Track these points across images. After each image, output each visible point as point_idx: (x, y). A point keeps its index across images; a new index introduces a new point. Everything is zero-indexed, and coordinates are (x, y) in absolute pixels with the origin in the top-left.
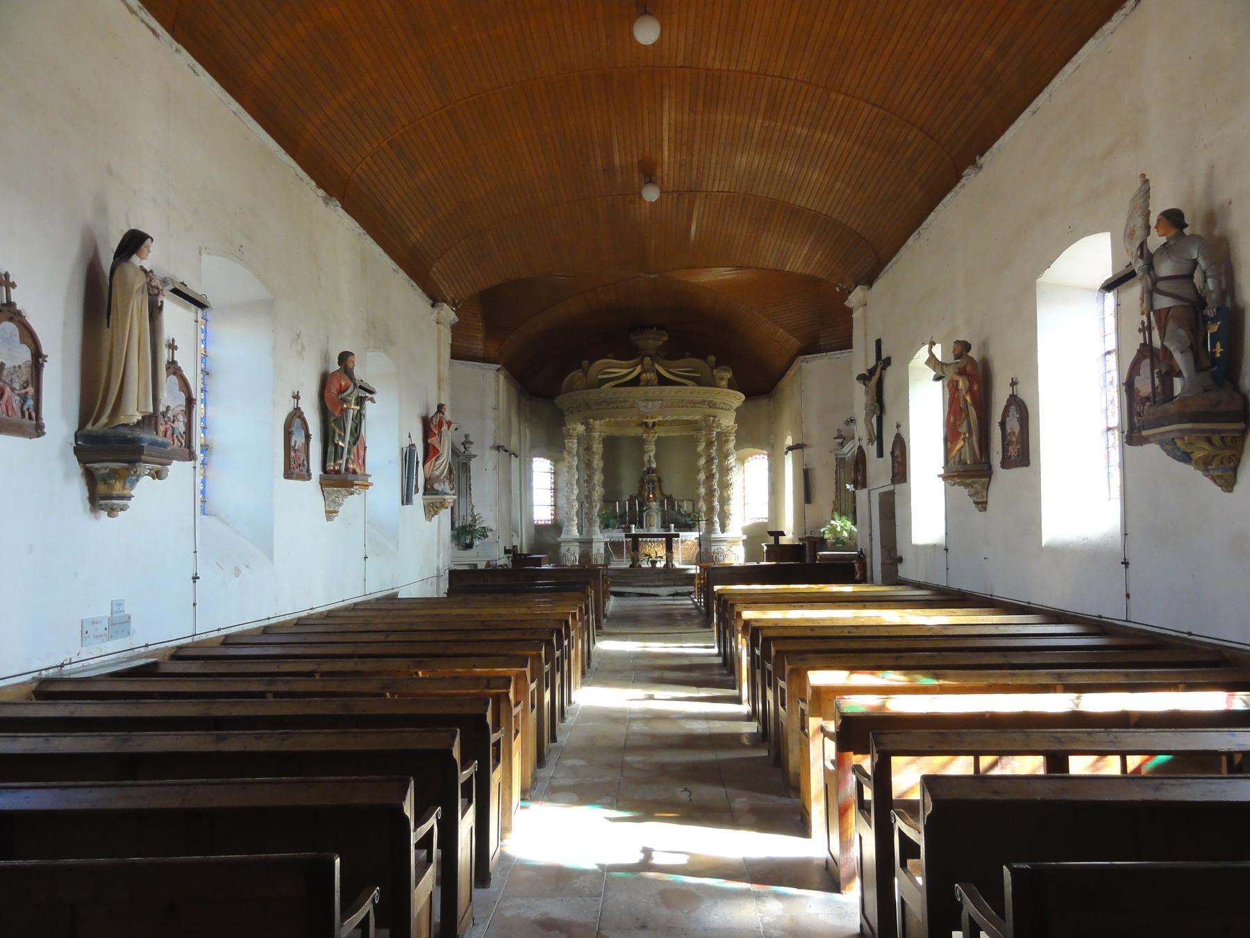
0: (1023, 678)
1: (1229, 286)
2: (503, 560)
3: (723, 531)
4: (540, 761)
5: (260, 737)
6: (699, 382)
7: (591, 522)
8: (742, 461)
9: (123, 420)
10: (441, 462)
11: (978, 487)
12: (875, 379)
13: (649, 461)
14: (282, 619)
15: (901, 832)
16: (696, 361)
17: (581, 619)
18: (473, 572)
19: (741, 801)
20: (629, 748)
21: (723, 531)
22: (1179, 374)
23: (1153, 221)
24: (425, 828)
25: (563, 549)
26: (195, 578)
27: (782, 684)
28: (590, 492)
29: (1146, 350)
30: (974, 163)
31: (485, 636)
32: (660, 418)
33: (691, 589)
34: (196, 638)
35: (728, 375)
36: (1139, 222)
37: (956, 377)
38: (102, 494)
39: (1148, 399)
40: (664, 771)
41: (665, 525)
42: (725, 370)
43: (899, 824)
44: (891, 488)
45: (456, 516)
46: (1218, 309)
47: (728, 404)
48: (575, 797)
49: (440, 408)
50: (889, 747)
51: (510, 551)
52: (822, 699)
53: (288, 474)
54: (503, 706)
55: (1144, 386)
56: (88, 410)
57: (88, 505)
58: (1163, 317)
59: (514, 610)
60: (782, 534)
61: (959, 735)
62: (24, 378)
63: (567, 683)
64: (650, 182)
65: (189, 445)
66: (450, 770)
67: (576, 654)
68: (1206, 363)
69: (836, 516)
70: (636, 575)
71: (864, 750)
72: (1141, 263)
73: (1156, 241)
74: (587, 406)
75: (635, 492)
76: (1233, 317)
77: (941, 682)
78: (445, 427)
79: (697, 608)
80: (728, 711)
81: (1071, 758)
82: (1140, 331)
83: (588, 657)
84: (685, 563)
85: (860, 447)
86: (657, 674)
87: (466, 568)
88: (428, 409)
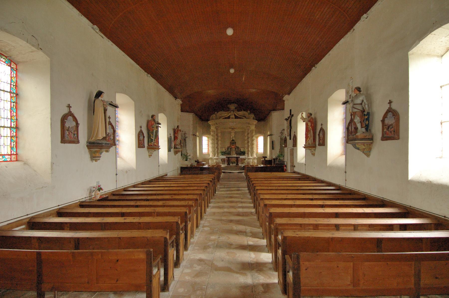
10: (178, 142)
11: (313, 150)
16: (245, 112)
26: (116, 175)
49: (178, 126)
60: (266, 157)
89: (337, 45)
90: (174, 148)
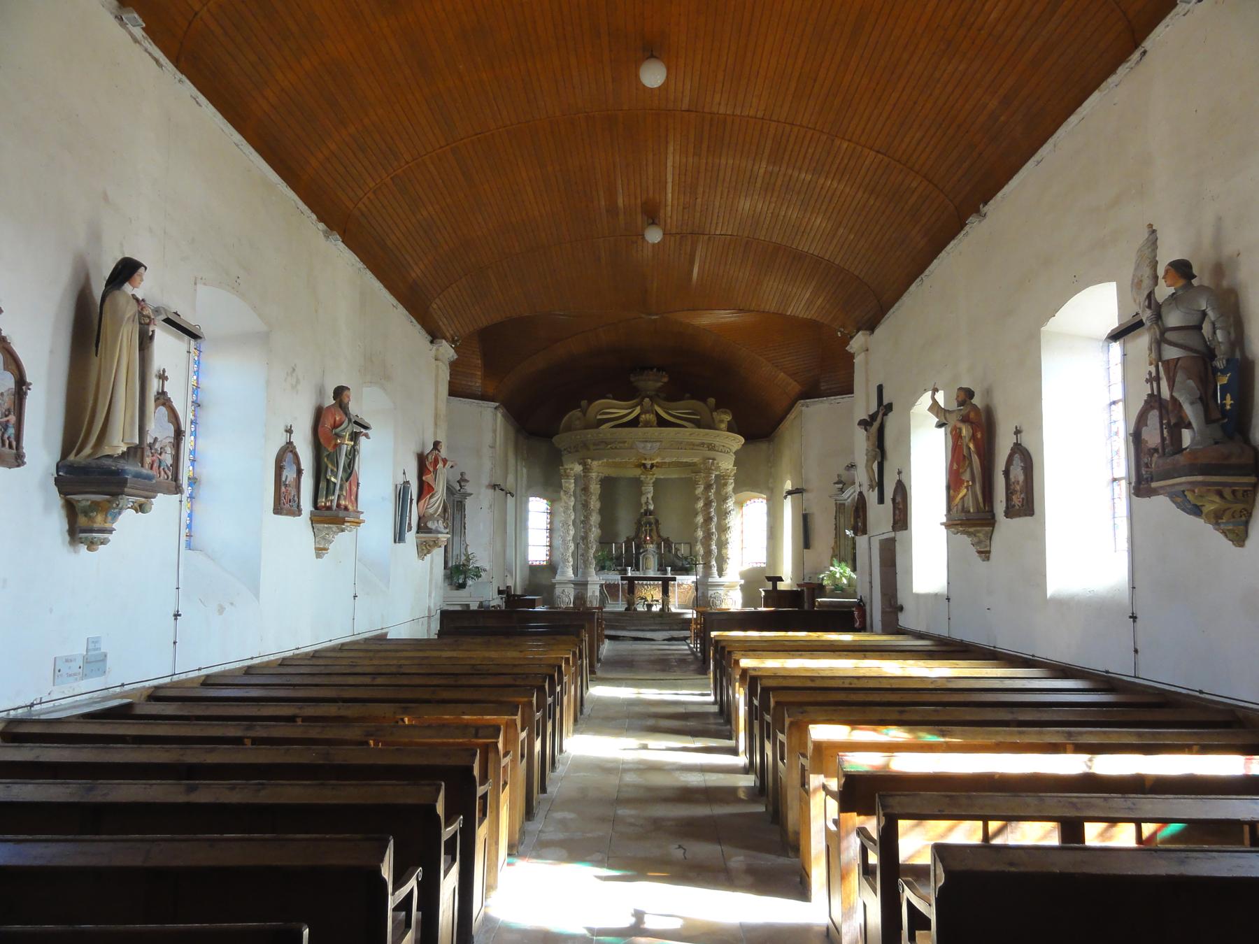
0: (1032, 735)
1: (1238, 338)
2: (496, 601)
3: (720, 575)
4: (529, 813)
5: (233, 788)
6: (698, 424)
7: (586, 564)
8: (740, 504)
9: (107, 451)
10: (433, 499)
12: (876, 425)
13: (647, 503)
14: (266, 659)
15: (909, 902)
16: (698, 404)
17: (575, 664)
18: (466, 613)
19: (738, 860)
20: (620, 801)
21: (720, 575)
22: (1189, 426)
23: (1161, 272)
24: (404, 891)
25: (558, 591)
26: (177, 615)
27: (781, 737)
28: (586, 533)
29: (1154, 401)
30: (978, 211)
31: (475, 681)
32: (658, 460)
33: (686, 633)
34: (175, 678)
35: (728, 418)
36: (1147, 272)
37: (960, 425)
38: (82, 527)
39: (1156, 450)
40: (657, 825)
41: (662, 568)
42: (725, 413)
43: (907, 894)
44: (892, 535)
45: (450, 555)
46: (1228, 361)
47: (727, 447)
48: (564, 853)
49: (436, 445)
50: (897, 810)
51: (505, 592)
52: (825, 755)
53: (278, 510)
54: (491, 756)
55: (1152, 436)
56: (71, 440)
57: (67, 538)
58: (1172, 368)
59: (505, 654)
60: (780, 579)
61: (969, 797)
62: (6, 406)
63: (558, 730)
64: (653, 223)
65: (176, 477)
66: (434, 826)
67: (568, 701)
68: (1216, 414)
69: (835, 562)
70: (631, 618)
71: (867, 811)
72: (1148, 313)
73: (1164, 291)
74: (585, 446)
75: (632, 534)
76: (1242, 369)
77: (948, 740)
78: (440, 465)
79: (693, 653)
80: (724, 763)
81: (1087, 825)
82: (1147, 381)
83: (580, 703)
84: (681, 607)
85: (861, 493)
86: (651, 722)
87: (458, 608)
88: (423, 445)
89: (1073, 119)
90: (419, 530)
